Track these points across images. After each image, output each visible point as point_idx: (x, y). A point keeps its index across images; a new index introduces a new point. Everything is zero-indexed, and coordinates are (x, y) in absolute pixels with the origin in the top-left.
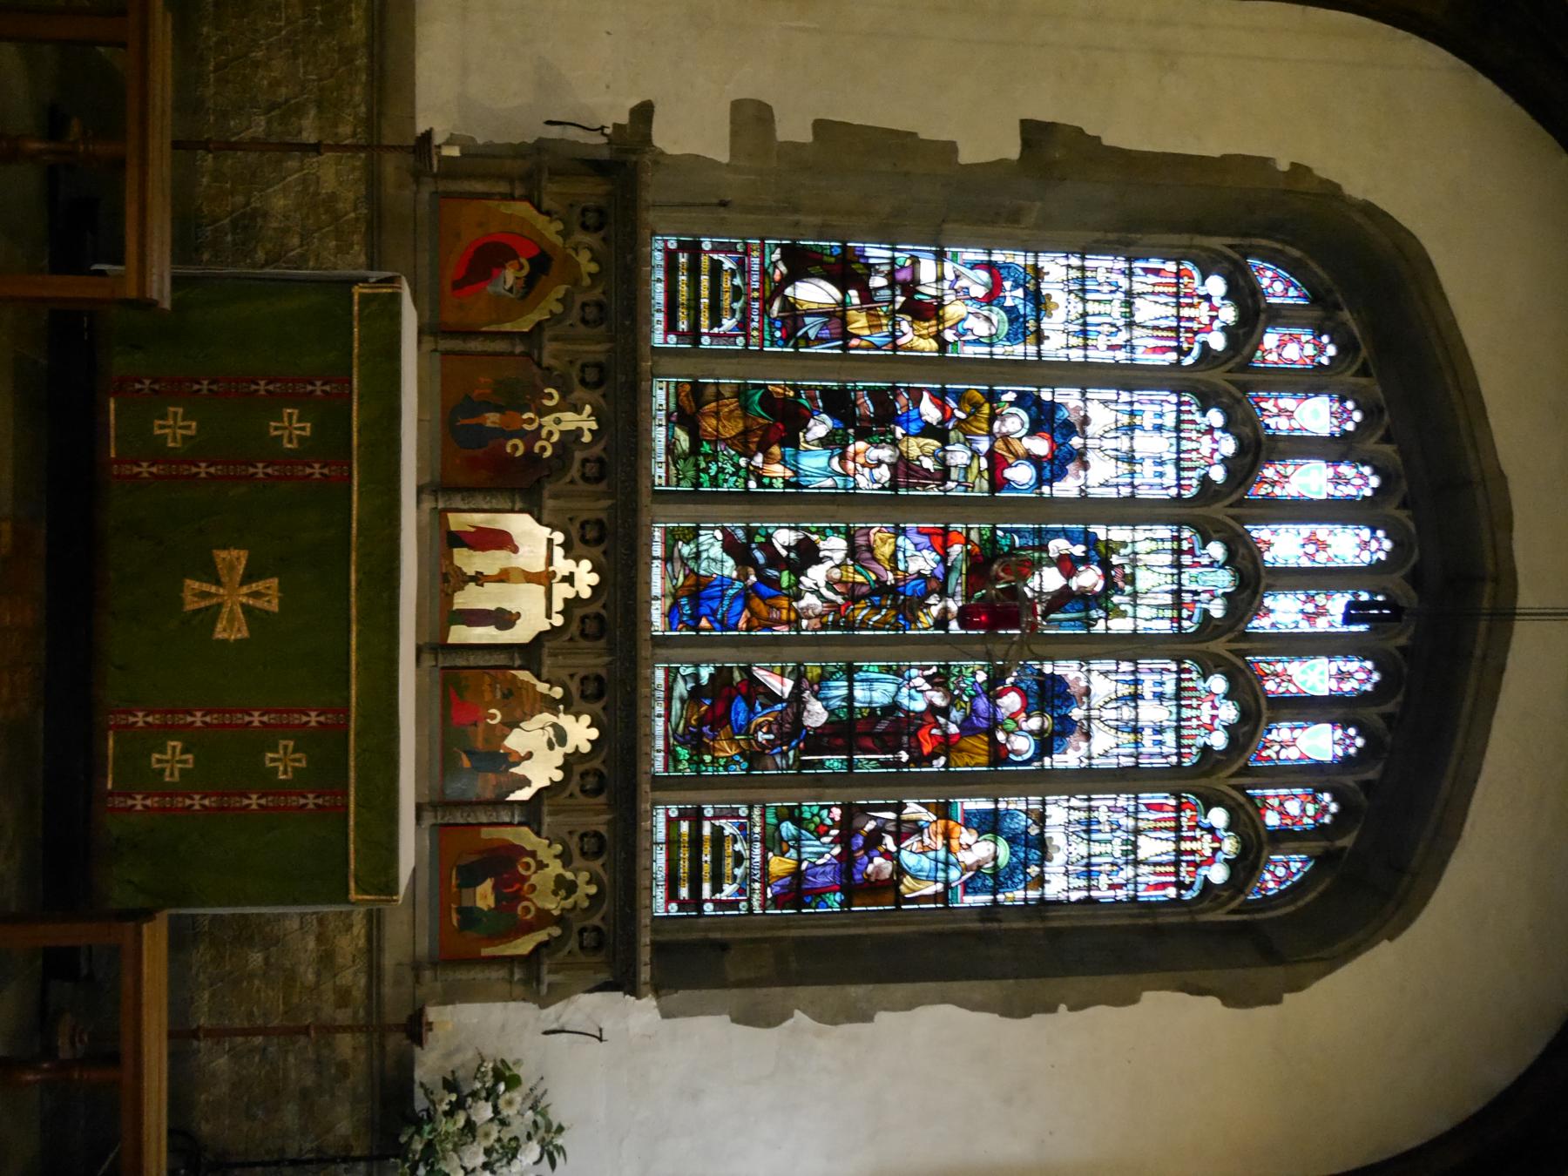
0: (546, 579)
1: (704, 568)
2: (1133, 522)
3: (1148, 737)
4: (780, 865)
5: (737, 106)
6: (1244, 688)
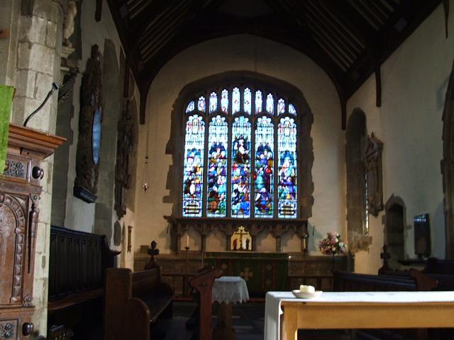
0: (241, 234)
1: (239, 208)
2: (231, 135)
3: (268, 133)
4: (288, 196)
5: (164, 202)
6: (261, 115)
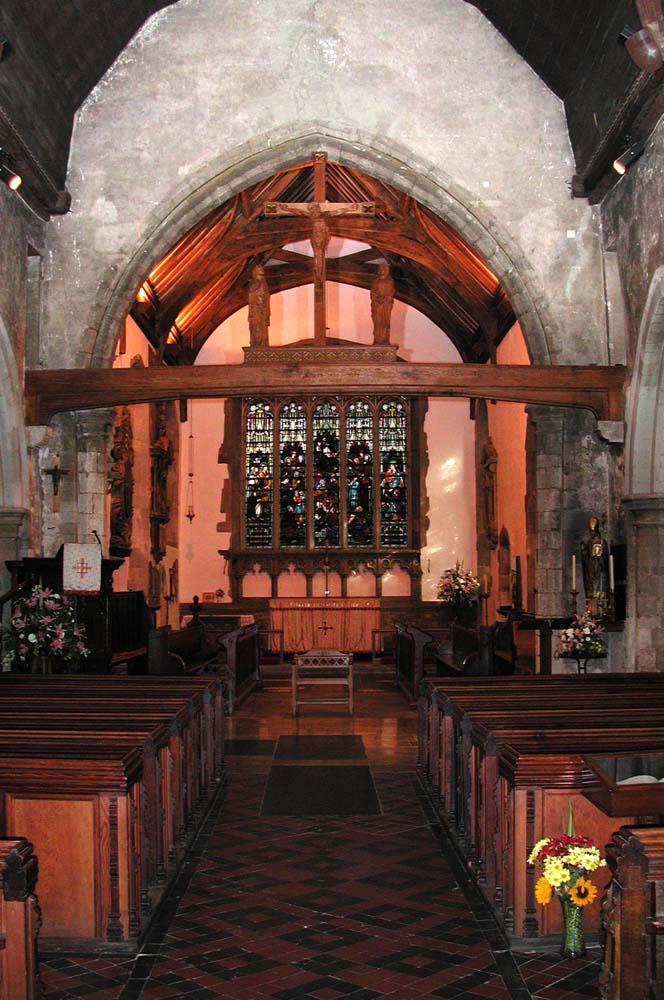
4: (395, 517)
